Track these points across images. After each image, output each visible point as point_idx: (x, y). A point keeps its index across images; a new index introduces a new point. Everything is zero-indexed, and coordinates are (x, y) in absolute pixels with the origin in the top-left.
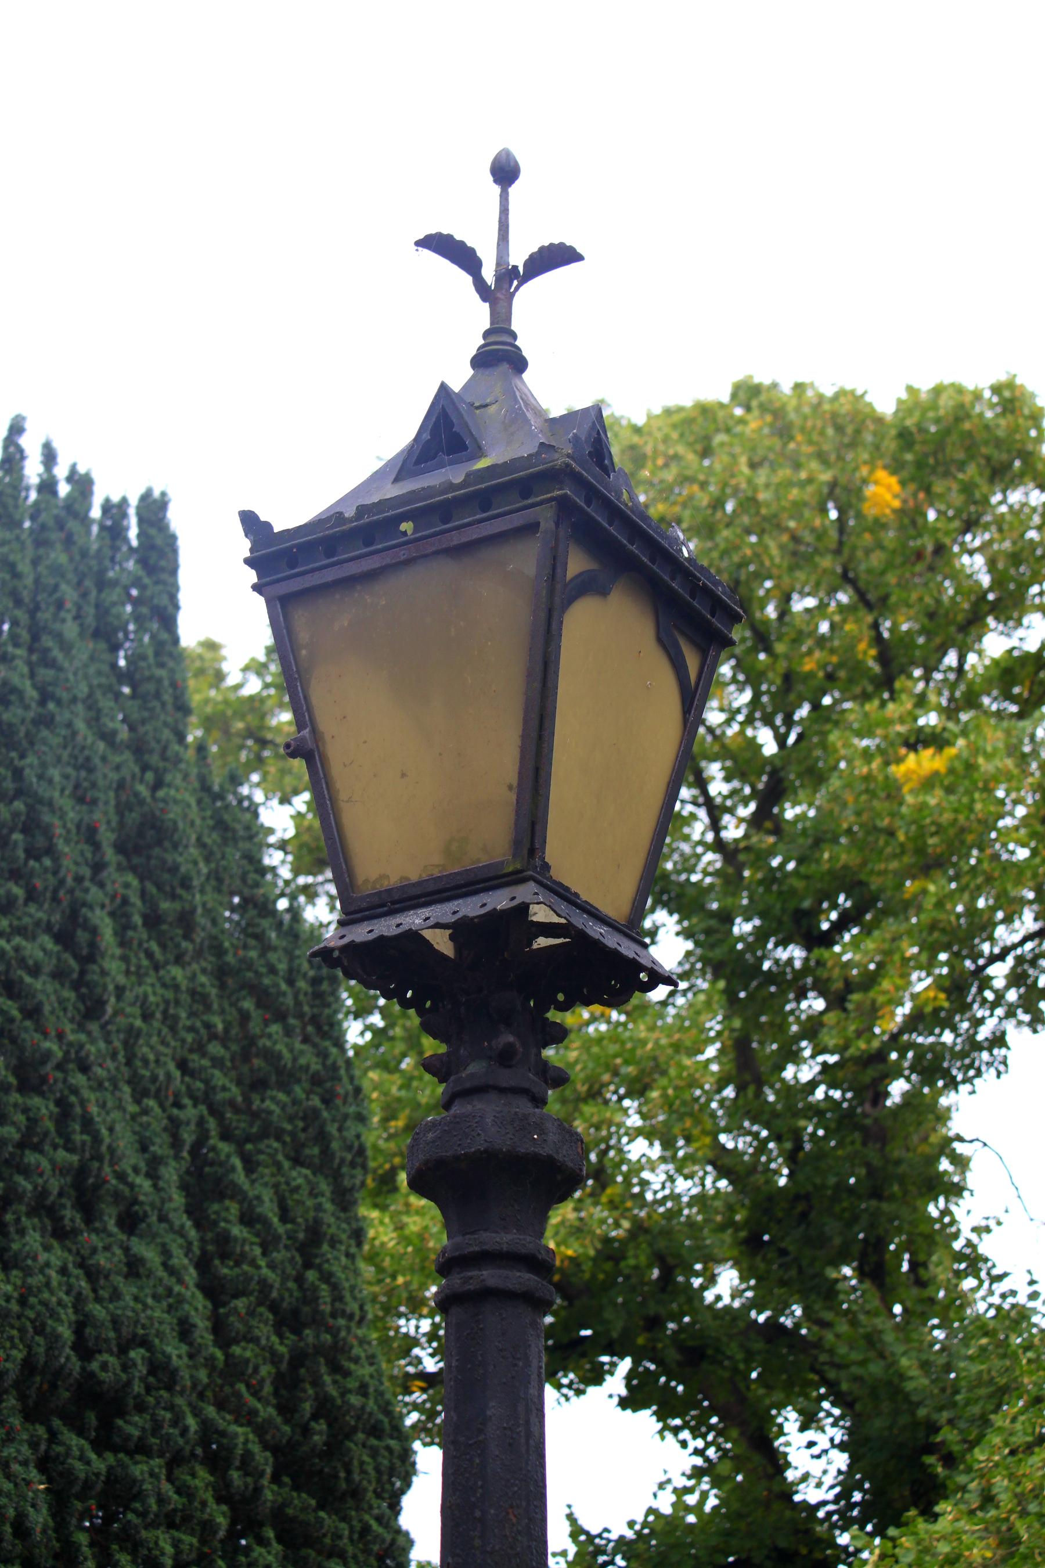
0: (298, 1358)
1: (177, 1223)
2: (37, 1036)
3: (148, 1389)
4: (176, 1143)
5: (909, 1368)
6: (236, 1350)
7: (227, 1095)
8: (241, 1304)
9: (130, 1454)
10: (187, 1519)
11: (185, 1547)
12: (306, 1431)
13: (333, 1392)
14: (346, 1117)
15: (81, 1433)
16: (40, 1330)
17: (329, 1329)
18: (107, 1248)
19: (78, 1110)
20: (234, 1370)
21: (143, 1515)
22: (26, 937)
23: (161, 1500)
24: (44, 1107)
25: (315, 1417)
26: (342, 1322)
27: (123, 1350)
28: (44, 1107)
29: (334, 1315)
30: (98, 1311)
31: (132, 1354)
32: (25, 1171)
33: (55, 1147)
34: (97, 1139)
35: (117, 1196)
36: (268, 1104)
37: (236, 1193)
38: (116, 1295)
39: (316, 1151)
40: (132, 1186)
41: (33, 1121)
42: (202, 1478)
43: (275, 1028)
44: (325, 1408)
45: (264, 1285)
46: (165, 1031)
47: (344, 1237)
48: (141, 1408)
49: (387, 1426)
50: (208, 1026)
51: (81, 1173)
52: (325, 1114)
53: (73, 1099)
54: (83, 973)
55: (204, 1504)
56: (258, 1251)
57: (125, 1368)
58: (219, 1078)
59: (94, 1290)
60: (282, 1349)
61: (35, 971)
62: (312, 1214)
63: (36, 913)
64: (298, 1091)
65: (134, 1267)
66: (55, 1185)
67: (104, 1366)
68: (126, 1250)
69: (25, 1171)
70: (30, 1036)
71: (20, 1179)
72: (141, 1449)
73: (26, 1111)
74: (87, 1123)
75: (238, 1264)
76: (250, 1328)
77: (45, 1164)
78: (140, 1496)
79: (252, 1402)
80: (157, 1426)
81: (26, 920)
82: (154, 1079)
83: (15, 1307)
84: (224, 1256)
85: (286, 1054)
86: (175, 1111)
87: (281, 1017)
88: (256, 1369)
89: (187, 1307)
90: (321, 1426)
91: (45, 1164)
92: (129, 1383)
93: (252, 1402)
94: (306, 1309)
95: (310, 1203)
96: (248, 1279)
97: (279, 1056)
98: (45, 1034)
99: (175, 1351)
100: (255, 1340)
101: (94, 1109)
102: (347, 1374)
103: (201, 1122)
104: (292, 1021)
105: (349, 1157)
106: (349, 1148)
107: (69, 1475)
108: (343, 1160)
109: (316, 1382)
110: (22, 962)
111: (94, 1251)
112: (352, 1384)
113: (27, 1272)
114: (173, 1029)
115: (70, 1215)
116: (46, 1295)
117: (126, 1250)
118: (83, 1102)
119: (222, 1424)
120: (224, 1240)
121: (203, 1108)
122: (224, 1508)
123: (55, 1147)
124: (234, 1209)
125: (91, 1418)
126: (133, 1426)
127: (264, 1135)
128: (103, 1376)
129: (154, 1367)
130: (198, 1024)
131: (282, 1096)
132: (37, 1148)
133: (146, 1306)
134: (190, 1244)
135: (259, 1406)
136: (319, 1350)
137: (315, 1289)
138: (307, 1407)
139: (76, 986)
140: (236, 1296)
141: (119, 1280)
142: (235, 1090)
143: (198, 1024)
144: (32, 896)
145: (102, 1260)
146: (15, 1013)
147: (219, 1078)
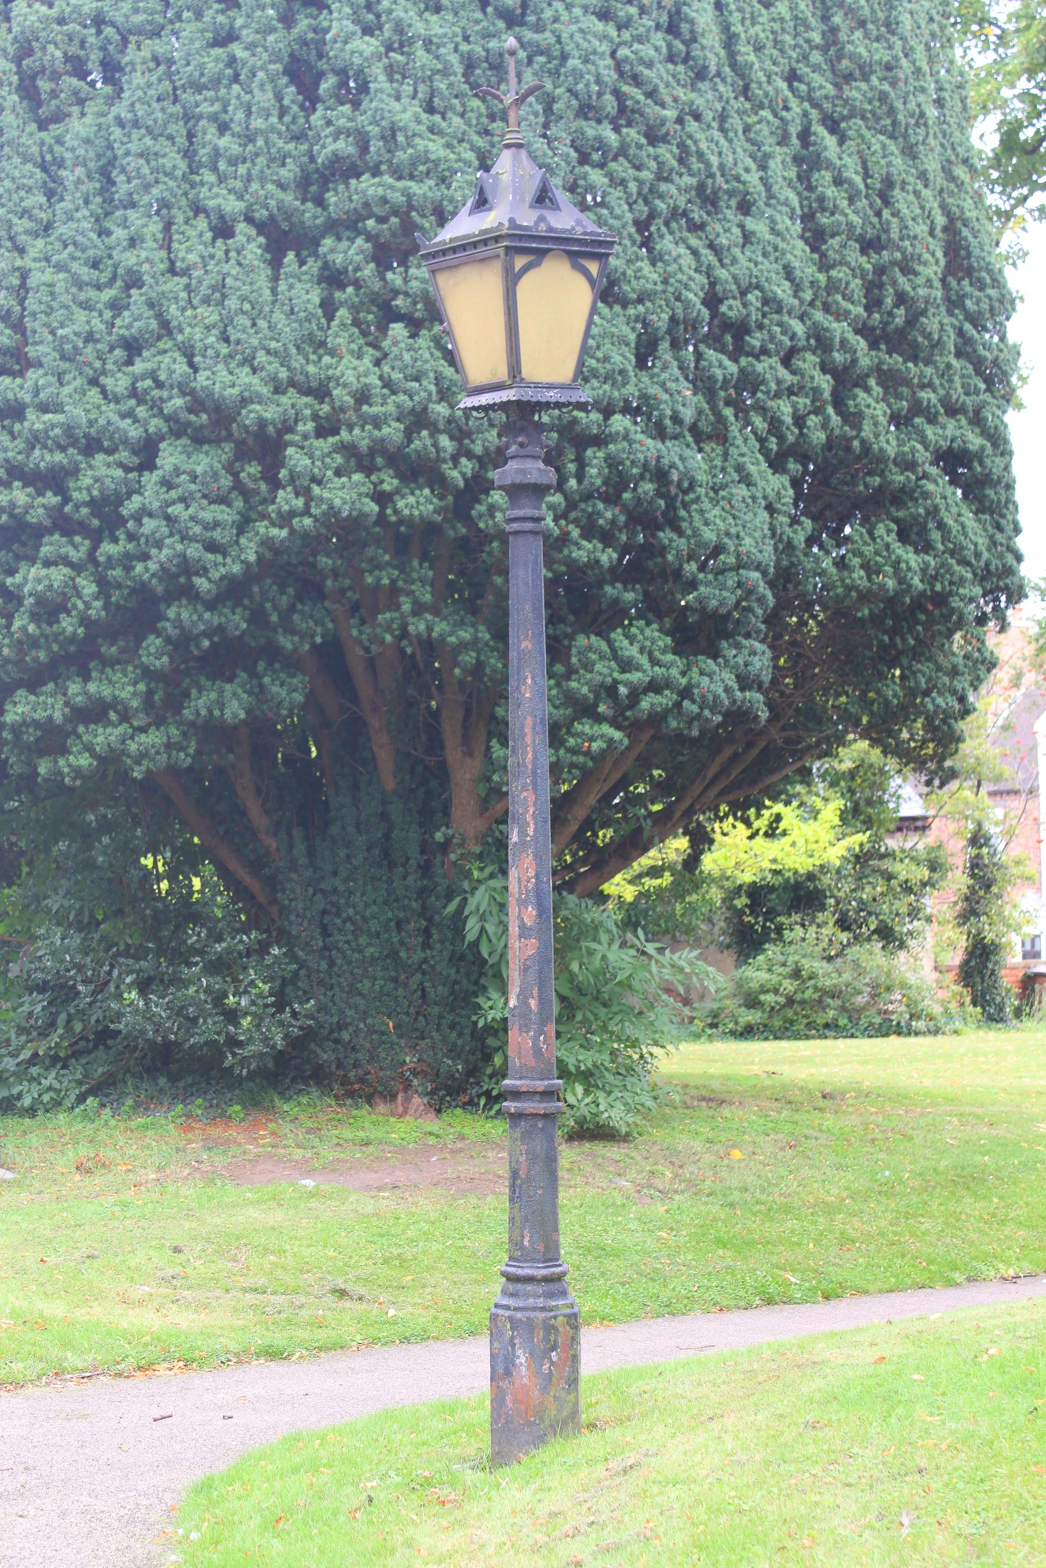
0: (880, 270)
1: (782, 198)
2: (658, 108)
3: (764, 315)
4: (783, 140)
5: (430, 629)
6: (834, 273)
7: (823, 92)
8: (835, 242)
9: (757, 357)
10: (801, 388)
11: (801, 407)
12: (890, 314)
13: (908, 288)
14: (907, 93)
15: (723, 351)
16: (678, 299)
17: (899, 248)
18: (727, 231)
19: (693, 148)
20: (832, 286)
21: (768, 393)
22: (641, 42)
23: (779, 382)
24: (667, 153)
25: (897, 306)
26: (907, 243)
27: (743, 293)
28: (667, 153)
29: (901, 239)
30: (722, 274)
31: (749, 296)
32: (661, 197)
33: (681, 175)
34: (708, 165)
35: (731, 194)
36: (855, 94)
37: (829, 165)
38: (734, 261)
39: (889, 121)
40: (744, 183)
41: (661, 165)
42: (809, 362)
43: (858, 34)
44: (901, 298)
45: (850, 225)
46: (775, 52)
47: (911, 180)
48: (760, 327)
49: (988, 281)
50: (808, 41)
51: (701, 188)
52: (893, 95)
53: (689, 142)
54: (688, 53)
55: (812, 378)
56: (845, 203)
57: (745, 305)
58: (817, 79)
59: (720, 261)
60: (869, 267)
61: (650, 65)
62: (884, 172)
63: (648, 22)
64: (874, 80)
65: (747, 237)
66: (682, 201)
67: (730, 308)
68: (742, 226)
69: (661, 197)
70: (652, 110)
71: (657, 202)
72: (764, 351)
73: (656, 158)
74: (700, 155)
75: (833, 214)
76: (843, 257)
77: (674, 191)
78: (764, 382)
79: (846, 305)
80: (772, 338)
81: (642, 30)
82: (766, 94)
83: (660, 287)
84: (823, 210)
85: (865, 54)
86: (784, 113)
87: (862, 24)
88: (848, 283)
89: (789, 256)
90: (901, 311)
91: (674, 191)
92: (748, 315)
93: (846, 305)
94: (884, 237)
95: (883, 162)
96: (840, 224)
97: (860, 56)
98: (663, 105)
99: (782, 290)
100: (847, 264)
101: (703, 146)
102: (916, 274)
103: (805, 114)
104: (870, 26)
105: (912, 121)
106: (912, 115)
107: (712, 378)
108: (907, 125)
109: (894, 283)
110: (641, 61)
111: (718, 235)
112: (920, 280)
113: (666, 263)
114: (782, 51)
115: (697, 214)
116: (680, 276)
117: (742, 226)
118: (695, 142)
119: (826, 324)
120: (822, 199)
121: (806, 105)
122: (828, 377)
123: (681, 175)
124: (827, 176)
125: (728, 338)
126: (755, 341)
127: (852, 116)
128: (730, 314)
129: (765, 302)
130: (801, 42)
131: (863, 86)
132: (667, 180)
133: (756, 264)
134: (793, 210)
135: (851, 307)
136: (894, 263)
137: (888, 222)
138: (889, 301)
139: (685, 61)
140: (833, 236)
141: (737, 252)
142: (829, 87)
143: (801, 42)
144: (643, 11)
145: (723, 240)
146: (641, 97)
147: (817, 79)
